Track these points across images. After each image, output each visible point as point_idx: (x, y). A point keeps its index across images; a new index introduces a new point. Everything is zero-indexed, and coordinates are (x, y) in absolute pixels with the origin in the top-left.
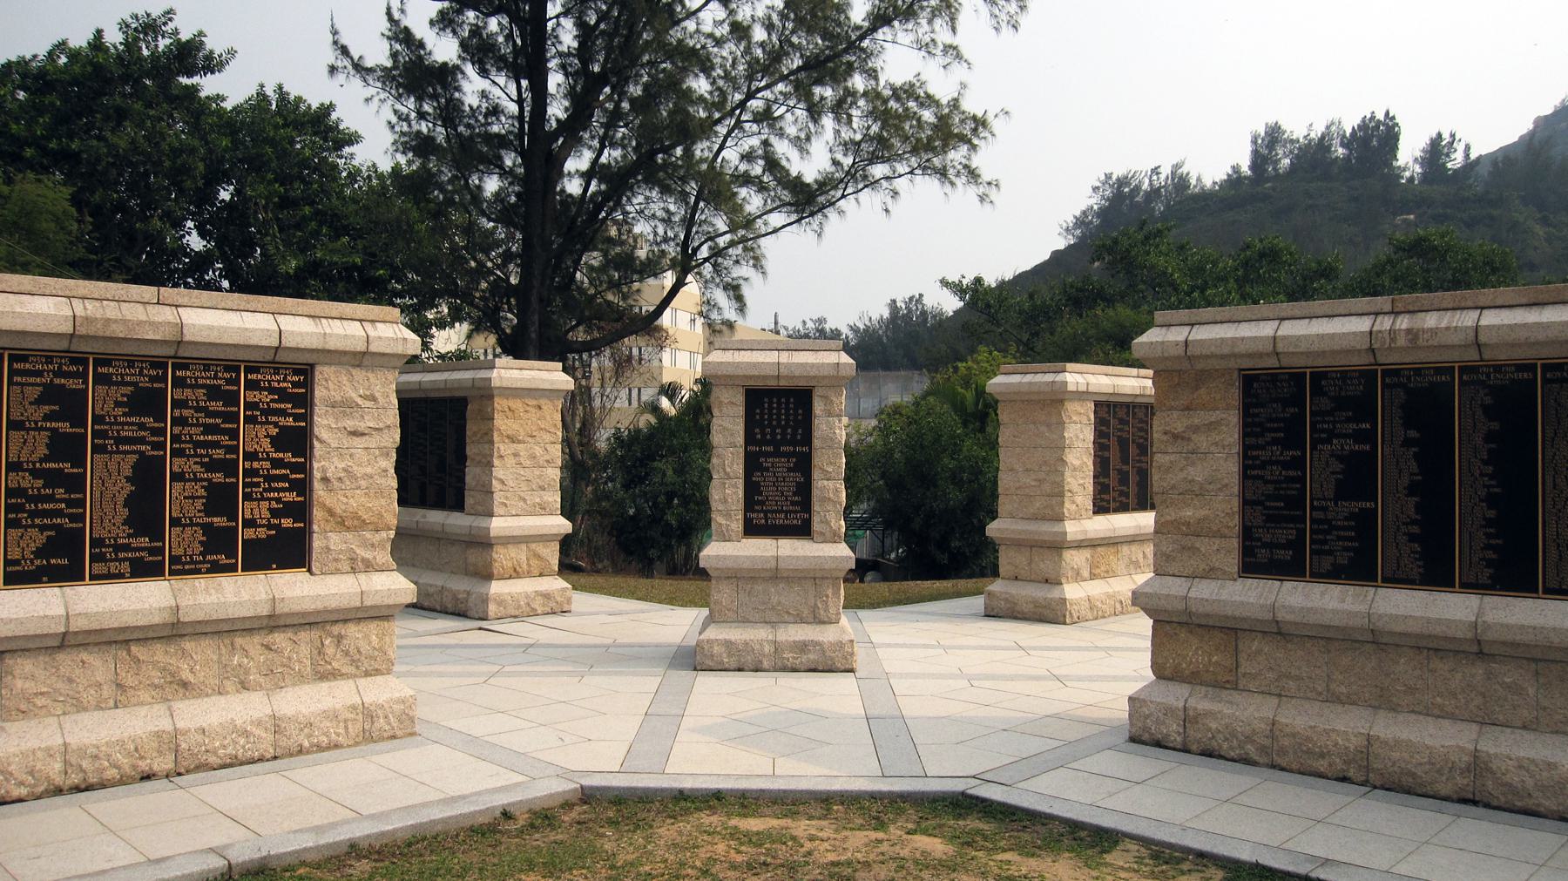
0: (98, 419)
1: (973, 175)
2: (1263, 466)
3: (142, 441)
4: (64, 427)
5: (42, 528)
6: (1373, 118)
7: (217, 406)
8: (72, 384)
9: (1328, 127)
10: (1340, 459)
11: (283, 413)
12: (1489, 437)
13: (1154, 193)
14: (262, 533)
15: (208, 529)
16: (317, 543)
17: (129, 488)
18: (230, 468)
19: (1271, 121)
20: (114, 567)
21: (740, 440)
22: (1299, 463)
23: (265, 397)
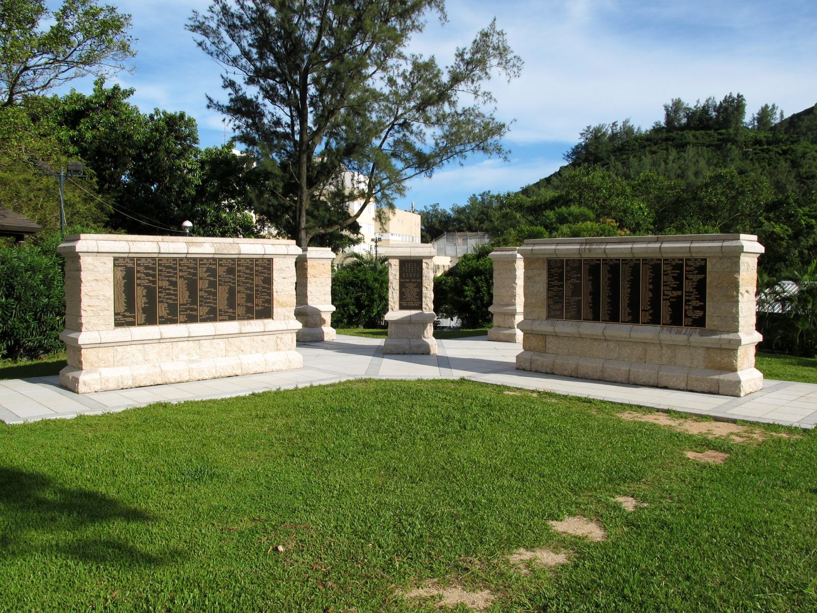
0: (219, 276)
1: (499, 150)
2: (553, 286)
3: (230, 282)
4: (212, 279)
5: (208, 307)
6: (730, 97)
7: (248, 271)
8: (213, 267)
9: (707, 101)
10: (573, 284)
11: (264, 273)
12: (609, 279)
13: (614, 136)
14: (260, 308)
15: (246, 306)
16: (275, 310)
17: (227, 295)
18: (252, 289)
19: (676, 97)
20: (224, 317)
21: (398, 277)
22: (562, 286)
23: (260, 268)
